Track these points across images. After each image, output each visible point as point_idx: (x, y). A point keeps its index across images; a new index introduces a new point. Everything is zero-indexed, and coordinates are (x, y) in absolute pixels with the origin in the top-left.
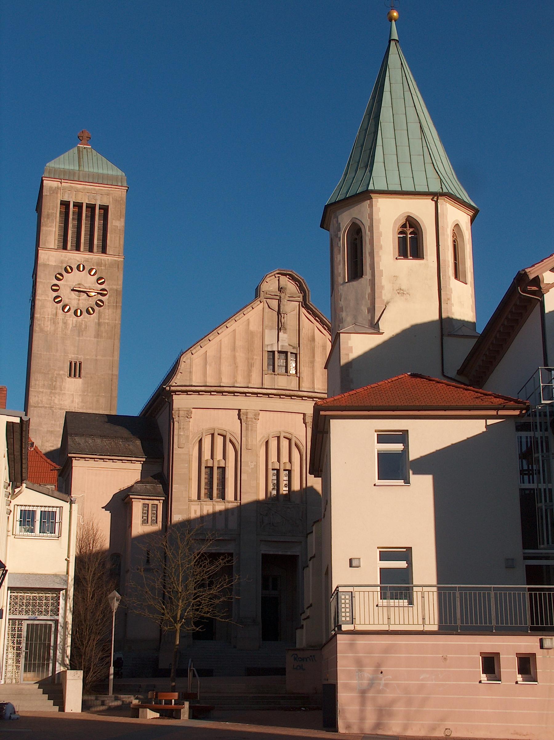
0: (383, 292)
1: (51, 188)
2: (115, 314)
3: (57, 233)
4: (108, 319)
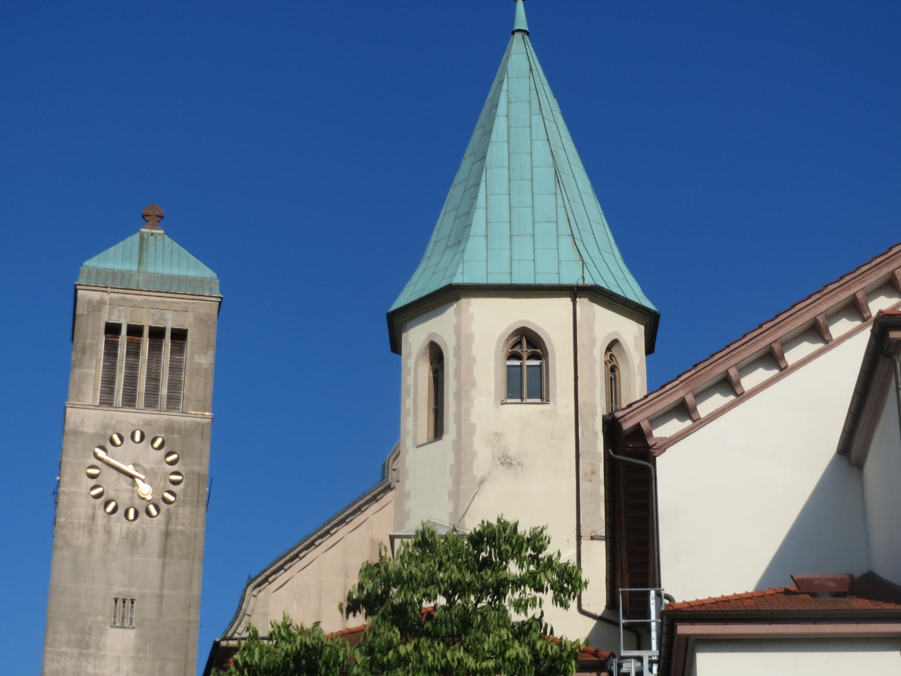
1: (90, 302)
2: (195, 515)
4: (183, 524)
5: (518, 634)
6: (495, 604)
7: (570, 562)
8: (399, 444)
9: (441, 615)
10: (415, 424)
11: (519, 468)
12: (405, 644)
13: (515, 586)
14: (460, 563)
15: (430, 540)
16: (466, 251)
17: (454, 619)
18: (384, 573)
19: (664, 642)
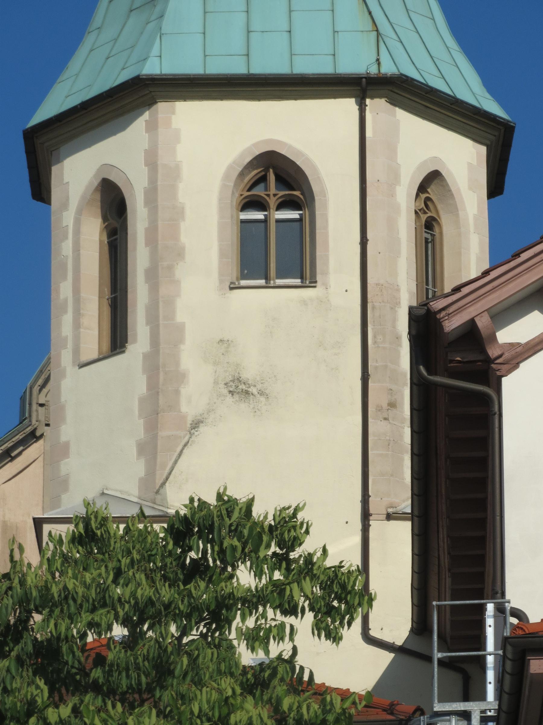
0: (185, 391)
5: (252, 685)
6: (212, 636)
7: (343, 564)
8: (48, 363)
9: (119, 658)
10: (77, 325)
11: (262, 399)
12: (57, 707)
13: (248, 607)
14: (151, 570)
15: (99, 532)
16: (166, 16)
17: (141, 664)
18: (18, 589)
19: (507, 688)
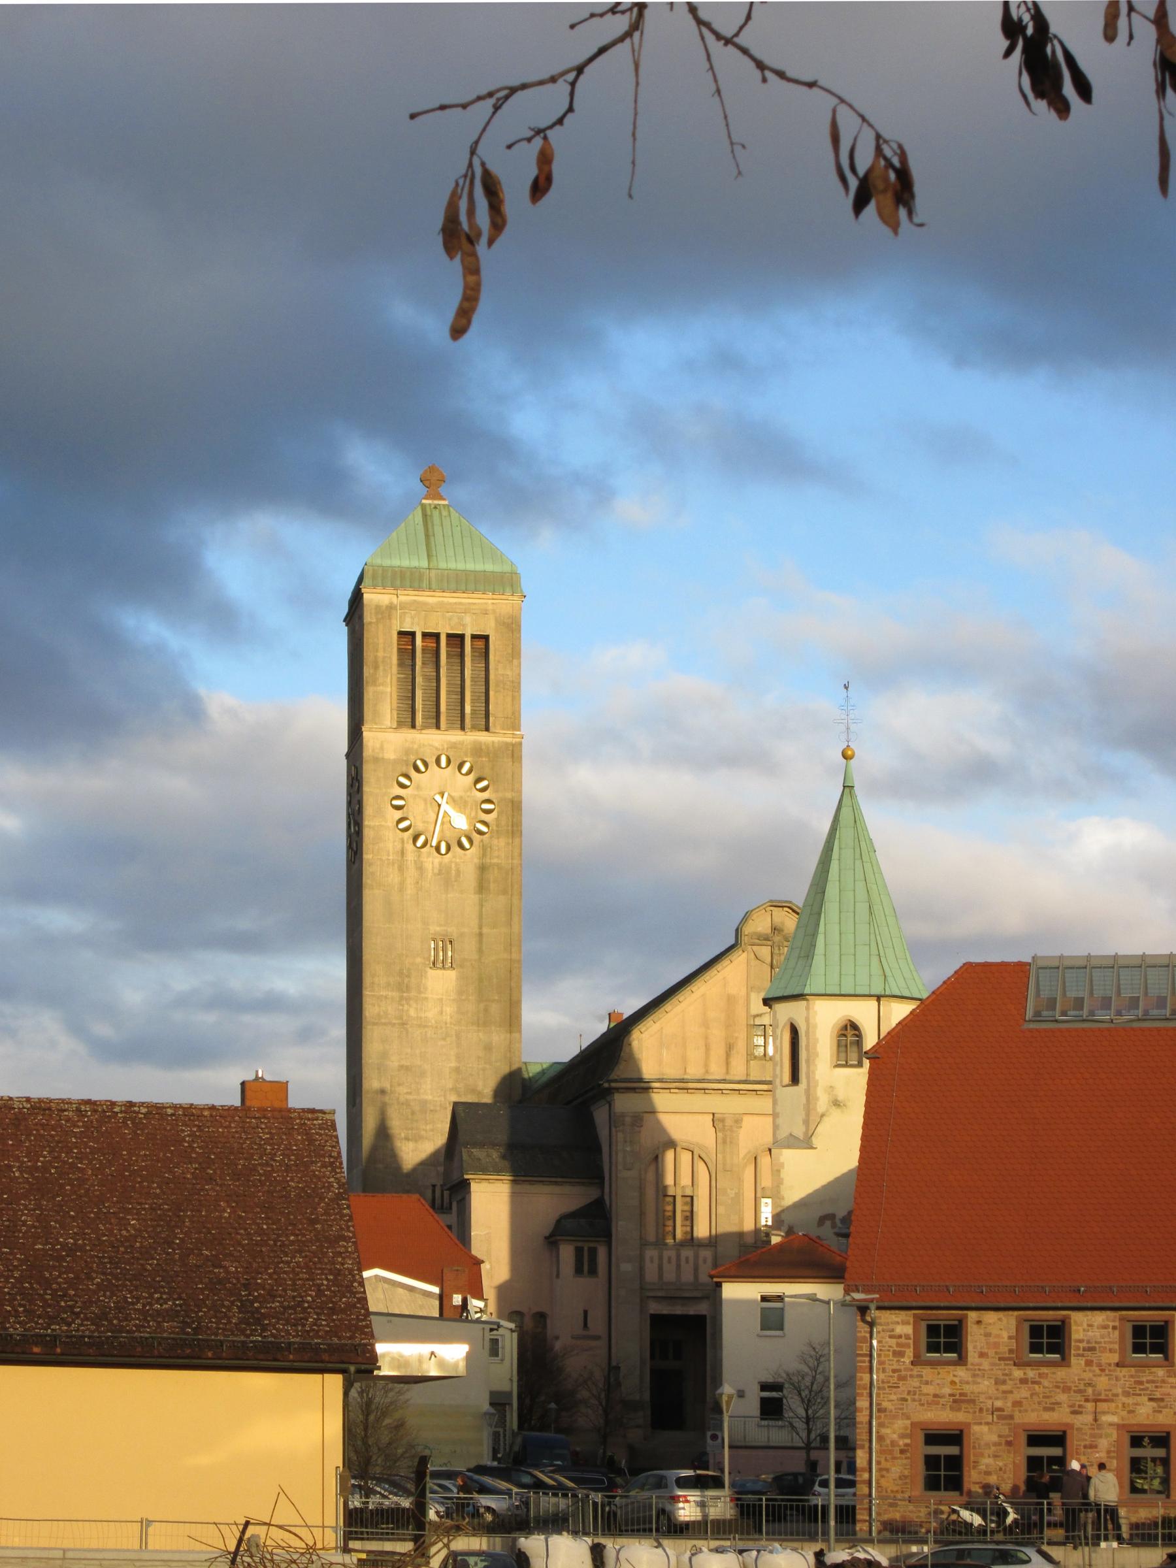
1: (378, 608)
3: (395, 696)
